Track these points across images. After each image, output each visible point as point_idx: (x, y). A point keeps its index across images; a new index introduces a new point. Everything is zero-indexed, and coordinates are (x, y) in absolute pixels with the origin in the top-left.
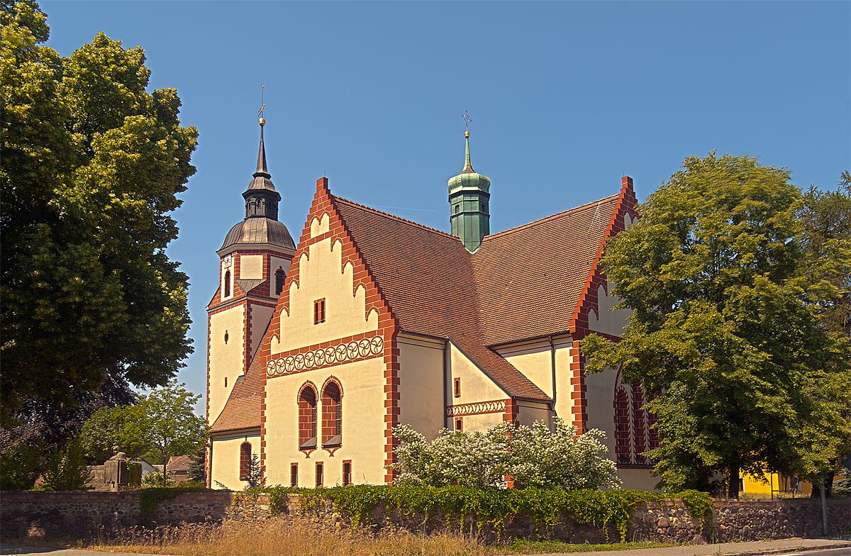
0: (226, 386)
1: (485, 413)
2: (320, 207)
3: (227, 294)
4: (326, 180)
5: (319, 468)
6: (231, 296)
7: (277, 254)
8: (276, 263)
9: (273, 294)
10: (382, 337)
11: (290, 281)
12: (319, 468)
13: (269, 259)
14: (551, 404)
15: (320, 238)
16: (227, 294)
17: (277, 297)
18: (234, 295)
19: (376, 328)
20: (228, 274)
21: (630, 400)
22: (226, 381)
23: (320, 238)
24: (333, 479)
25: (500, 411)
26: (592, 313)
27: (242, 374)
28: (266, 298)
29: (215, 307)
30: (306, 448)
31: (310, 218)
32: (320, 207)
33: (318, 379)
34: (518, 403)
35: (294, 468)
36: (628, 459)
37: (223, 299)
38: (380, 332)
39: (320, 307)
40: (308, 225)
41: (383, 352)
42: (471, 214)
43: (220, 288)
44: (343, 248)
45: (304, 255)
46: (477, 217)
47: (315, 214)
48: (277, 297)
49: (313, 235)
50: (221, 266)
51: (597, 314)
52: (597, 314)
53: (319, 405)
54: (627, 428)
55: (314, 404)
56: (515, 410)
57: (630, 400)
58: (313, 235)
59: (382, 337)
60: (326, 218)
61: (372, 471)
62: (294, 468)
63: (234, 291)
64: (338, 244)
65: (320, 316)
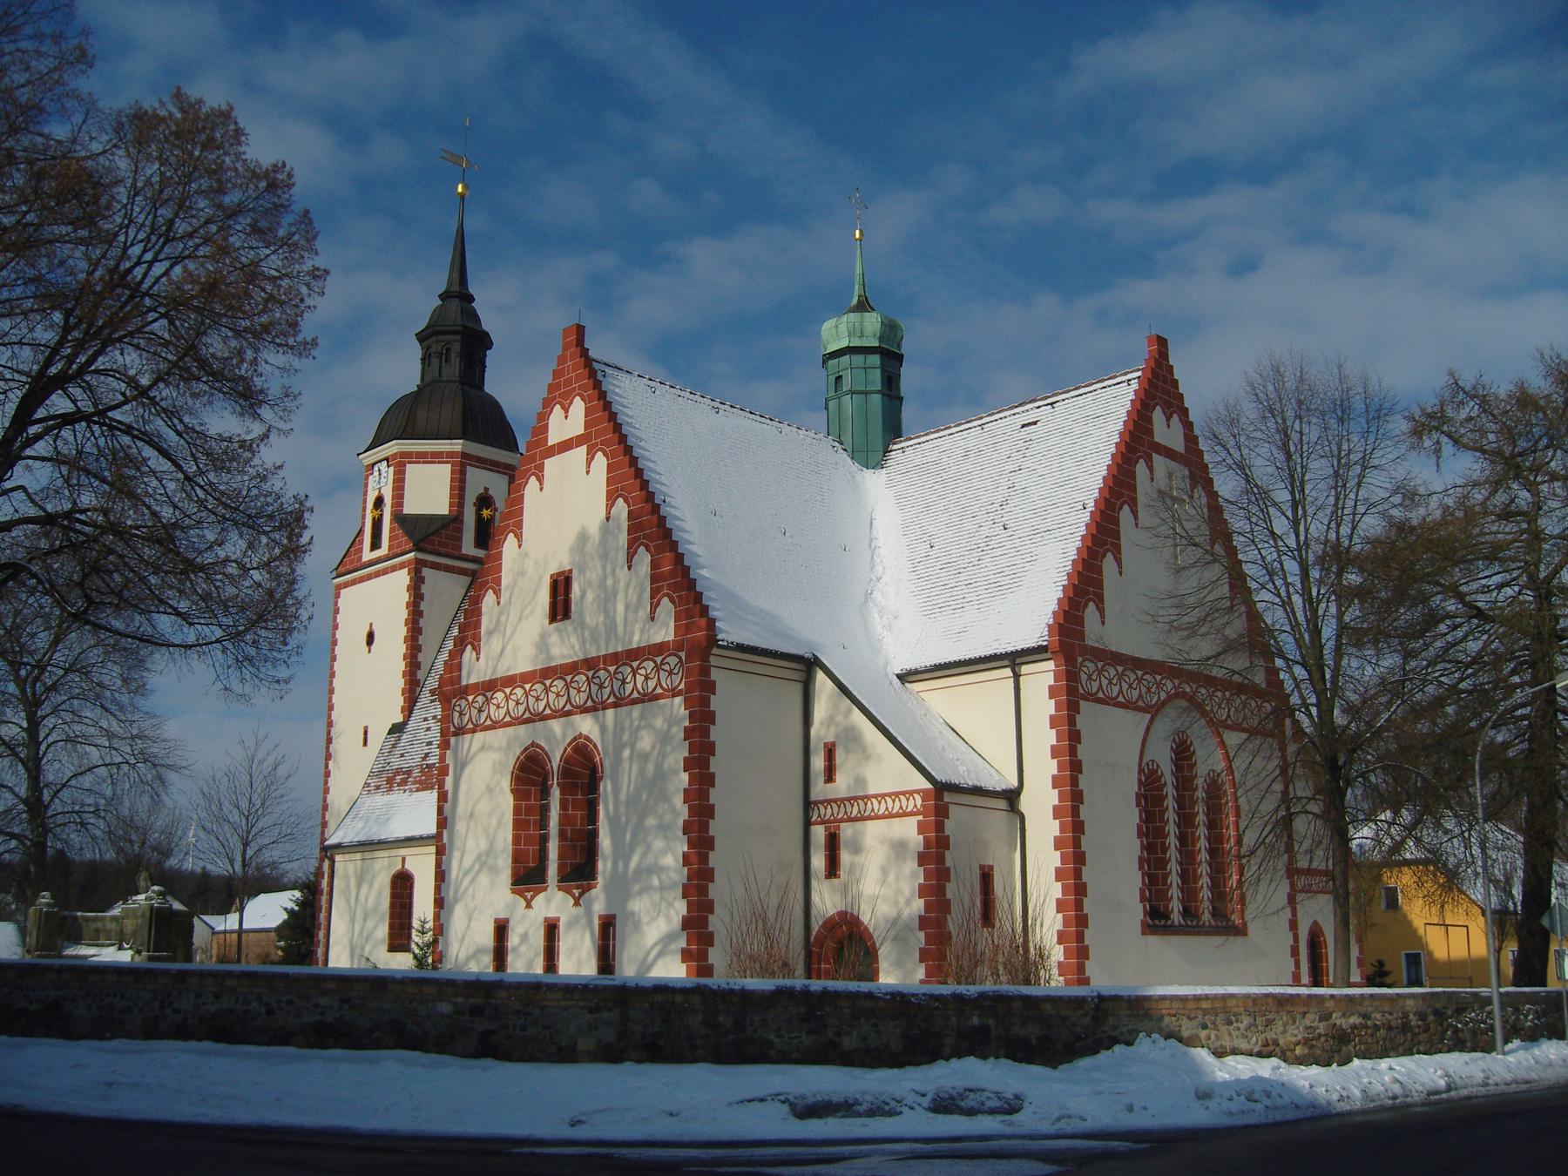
0: (365, 743)
1: (883, 817)
2: (568, 382)
3: (375, 545)
4: (580, 330)
5: (551, 929)
6: (383, 550)
7: (482, 463)
8: (479, 480)
9: (468, 546)
10: (683, 655)
11: (504, 532)
12: (551, 929)
13: (463, 473)
14: (1011, 797)
15: (566, 446)
16: (375, 545)
17: (481, 553)
18: (390, 548)
19: (671, 637)
20: (379, 502)
21: (1170, 790)
22: (366, 733)
23: (566, 446)
24: (577, 961)
25: (912, 814)
26: (1091, 612)
27: (399, 719)
28: (454, 550)
29: (349, 566)
30: (527, 877)
31: (548, 404)
32: (568, 382)
33: (556, 738)
34: (947, 797)
35: (501, 929)
36: (1166, 916)
37: (367, 555)
38: (678, 646)
39: (561, 587)
40: (543, 417)
41: (682, 686)
42: (866, 393)
43: (361, 532)
44: (610, 468)
45: (533, 479)
46: (877, 398)
47: (558, 395)
48: (481, 553)
49: (553, 439)
50: (366, 485)
51: (1119, 561)
52: (1119, 561)
53: (556, 793)
54: (1165, 849)
55: (545, 792)
56: (941, 812)
57: (1170, 790)
58: (553, 439)
59: (683, 655)
60: (578, 406)
61: (656, 954)
62: (501, 929)
63: (391, 539)
64: (600, 461)
65: (561, 604)
